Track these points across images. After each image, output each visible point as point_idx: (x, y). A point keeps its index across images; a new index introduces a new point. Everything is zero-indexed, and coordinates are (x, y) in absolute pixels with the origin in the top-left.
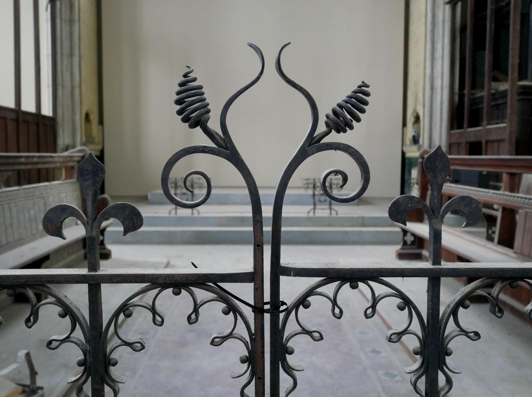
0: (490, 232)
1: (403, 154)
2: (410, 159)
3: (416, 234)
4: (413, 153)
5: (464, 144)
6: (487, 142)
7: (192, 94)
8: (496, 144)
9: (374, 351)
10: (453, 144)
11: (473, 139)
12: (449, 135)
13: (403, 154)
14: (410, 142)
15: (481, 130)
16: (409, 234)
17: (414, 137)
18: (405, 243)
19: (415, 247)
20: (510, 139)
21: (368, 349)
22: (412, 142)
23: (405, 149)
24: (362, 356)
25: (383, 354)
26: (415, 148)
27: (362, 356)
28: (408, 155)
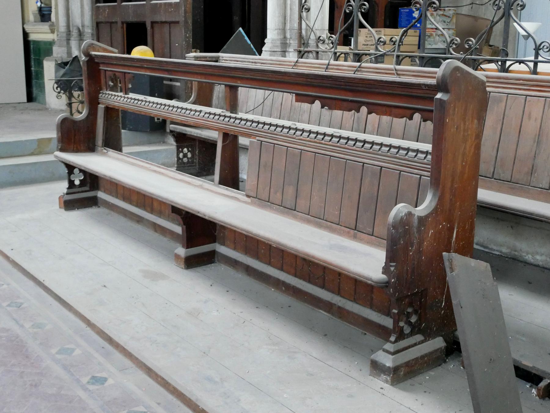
0: (181, 155)
1: (25, 35)
2: (36, 42)
3: (87, 170)
4: (40, 33)
5: (120, 24)
6: (153, 23)
7: (140, 69)
8: (166, 28)
9: (96, 380)
10: (102, 22)
11: (132, 19)
12: (96, 11)
13: (25, 35)
14: (35, 17)
15: (144, 4)
16: (76, 171)
17: (40, 9)
18: (71, 184)
19: (87, 188)
20: (186, 22)
21: (85, 380)
22: (38, 17)
23: (28, 28)
24: (81, 393)
25: (110, 381)
26: (45, 27)
27: (81, 393)
28: (33, 37)
